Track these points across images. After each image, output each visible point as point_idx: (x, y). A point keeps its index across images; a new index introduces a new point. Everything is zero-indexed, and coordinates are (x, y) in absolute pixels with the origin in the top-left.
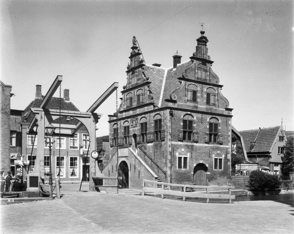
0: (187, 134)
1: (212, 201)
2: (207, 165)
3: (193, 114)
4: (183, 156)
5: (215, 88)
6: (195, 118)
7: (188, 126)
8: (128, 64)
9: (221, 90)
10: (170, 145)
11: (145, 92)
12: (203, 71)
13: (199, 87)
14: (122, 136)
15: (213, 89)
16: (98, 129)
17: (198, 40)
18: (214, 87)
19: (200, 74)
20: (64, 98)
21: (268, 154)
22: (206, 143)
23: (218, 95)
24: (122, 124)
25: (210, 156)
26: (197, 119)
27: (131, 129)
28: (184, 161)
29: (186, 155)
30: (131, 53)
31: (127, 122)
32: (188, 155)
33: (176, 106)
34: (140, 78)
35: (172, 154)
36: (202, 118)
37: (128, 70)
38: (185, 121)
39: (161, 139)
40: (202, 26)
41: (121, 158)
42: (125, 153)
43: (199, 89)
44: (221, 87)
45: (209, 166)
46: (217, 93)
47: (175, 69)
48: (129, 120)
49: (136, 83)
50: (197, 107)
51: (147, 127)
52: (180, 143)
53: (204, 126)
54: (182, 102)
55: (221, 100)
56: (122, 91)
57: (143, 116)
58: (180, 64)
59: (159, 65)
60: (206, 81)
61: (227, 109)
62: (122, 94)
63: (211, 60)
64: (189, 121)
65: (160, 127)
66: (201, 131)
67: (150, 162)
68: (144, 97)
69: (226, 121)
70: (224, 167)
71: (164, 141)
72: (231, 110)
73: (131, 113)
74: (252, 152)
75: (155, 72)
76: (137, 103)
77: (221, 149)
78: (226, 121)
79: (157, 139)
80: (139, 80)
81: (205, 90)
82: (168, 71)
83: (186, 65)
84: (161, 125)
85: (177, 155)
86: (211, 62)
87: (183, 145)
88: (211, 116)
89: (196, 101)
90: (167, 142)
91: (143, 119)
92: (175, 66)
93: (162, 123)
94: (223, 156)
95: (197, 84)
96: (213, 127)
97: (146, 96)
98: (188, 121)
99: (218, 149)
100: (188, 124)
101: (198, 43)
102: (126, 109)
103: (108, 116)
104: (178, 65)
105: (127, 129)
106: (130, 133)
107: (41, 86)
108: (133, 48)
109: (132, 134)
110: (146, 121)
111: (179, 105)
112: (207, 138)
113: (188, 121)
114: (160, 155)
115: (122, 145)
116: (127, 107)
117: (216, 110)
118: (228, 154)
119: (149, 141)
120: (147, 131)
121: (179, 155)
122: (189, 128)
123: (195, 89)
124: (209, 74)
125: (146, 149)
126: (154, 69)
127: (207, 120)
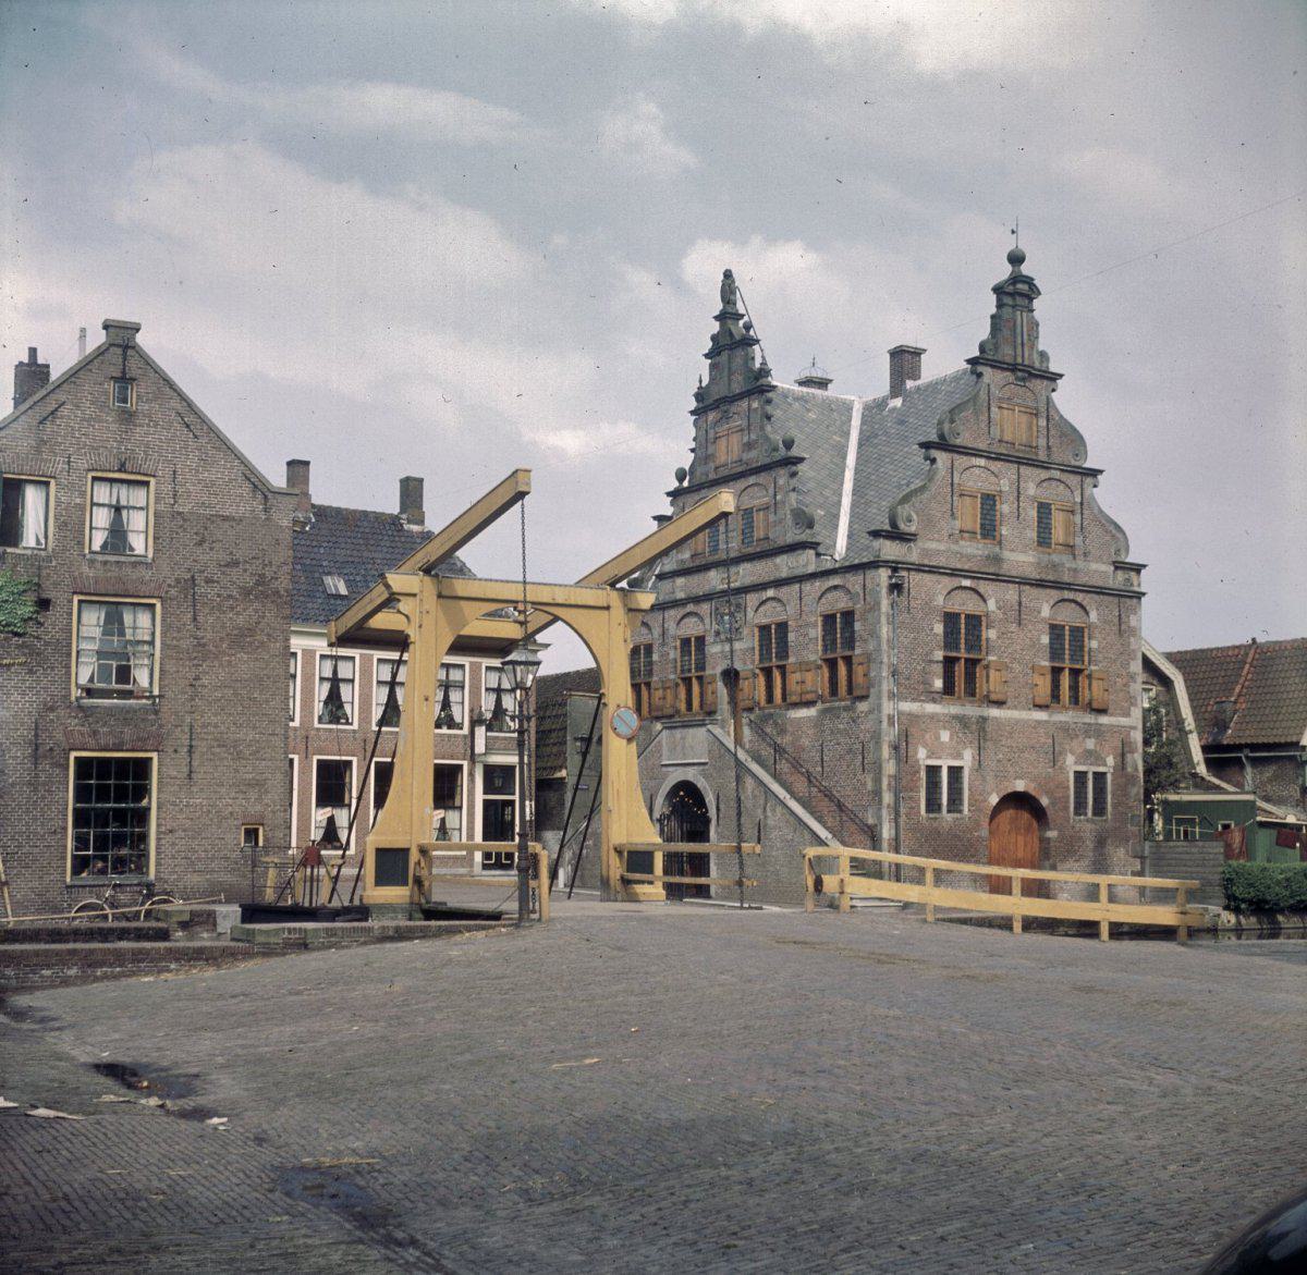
0: (960, 669)
1: (1119, 931)
2: (1044, 801)
3: (983, 587)
4: (945, 764)
5: (1073, 480)
6: (992, 605)
7: (963, 636)
8: (701, 381)
9: (1095, 486)
10: (891, 718)
11: (778, 497)
12: (1019, 411)
13: (1003, 479)
14: (672, 677)
15: (1062, 487)
16: (549, 645)
17: (998, 290)
18: (1064, 477)
19: (1012, 426)
20: (401, 513)
21: (1298, 753)
22: (1039, 707)
23: (1082, 509)
24: (671, 626)
25: (1055, 758)
26: (999, 609)
27: (714, 649)
28: (949, 783)
29: (959, 756)
30: (714, 338)
31: (696, 619)
32: (967, 760)
33: (913, 554)
34: (756, 442)
35: (901, 750)
36: (1020, 604)
37: (701, 405)
38: (951, 619)
39: (850, 690)
40: (1013, 232)
41: (364, 772)
42: (692, 747)
43: (1005, 485)
44: (1095, 476)
45: (1053, 803)
46: (1078, 500)
47: (898, 402)
48: (705, 608)
49: (735, 458)
50: (997, 560)
51: (786, 643)
52: (931, 708)
53: (1029, 635)
54: (938, 541)
55: (1095, 532)
56: (672, 489)
57: (770, 593)
58: (918, 382)
59: (823, 384)
60: (1037, 454)
61: (1119, 566)
62: (672, 504)
63: (1054, 368)
64: (967, 616)
65: (850, 642)
66: (1015, 659)
67: (801, 785)
68: (772, 518)
69: (1120, 615)
70: (1115, 806)
71: (864, 698)
72: (1138, 569)
73: (714, 580)
74: (1225, 743)
75: (812, 415)
76: (743, 540)
77: (1098, 732)
78: (1120, 615)
79: (834, 691)
80: (749, 446)
81: (1031, 489)
82: (867, 408)
83: (949, 389)
84: (853, 632)
85: (922, 756)
86: (1054, 377)
87: (945, 715)
88: (1055, 595)
89: (994, 537)
90: (879, 706)
91: (769, 605)
92: (897, 388)
93: (857, 626)
94: (1110, 761)
95: (996, 466)
96: (1067, 642)
97: (780, 512)
98: (963, 616)
99: (1089, 731)
100: (963, 631)
101: (998, 300)
102: (689, 565)
103: (655, 518)
104: (910, 384)
105: (694, 646)
106: (709, 662)
107: (307, 463)
108: (720, 318)
109: (719, 670)
110: (782, 618)
111: (926, 552)
112: (1044, 685)
113: (963, 616)
114: (848, 757)
115: (671, 716)
116: (692, 556)
117: (1075, 570)
118: (1132, 752)
119: (795, 698)
120: (787, 657)
121: (928, 757)
122: (970, 648)
123: (990, 488)
124: (1045, 424)
125: (782, 732)
126: (806, 401)
127: (1039, 612)
